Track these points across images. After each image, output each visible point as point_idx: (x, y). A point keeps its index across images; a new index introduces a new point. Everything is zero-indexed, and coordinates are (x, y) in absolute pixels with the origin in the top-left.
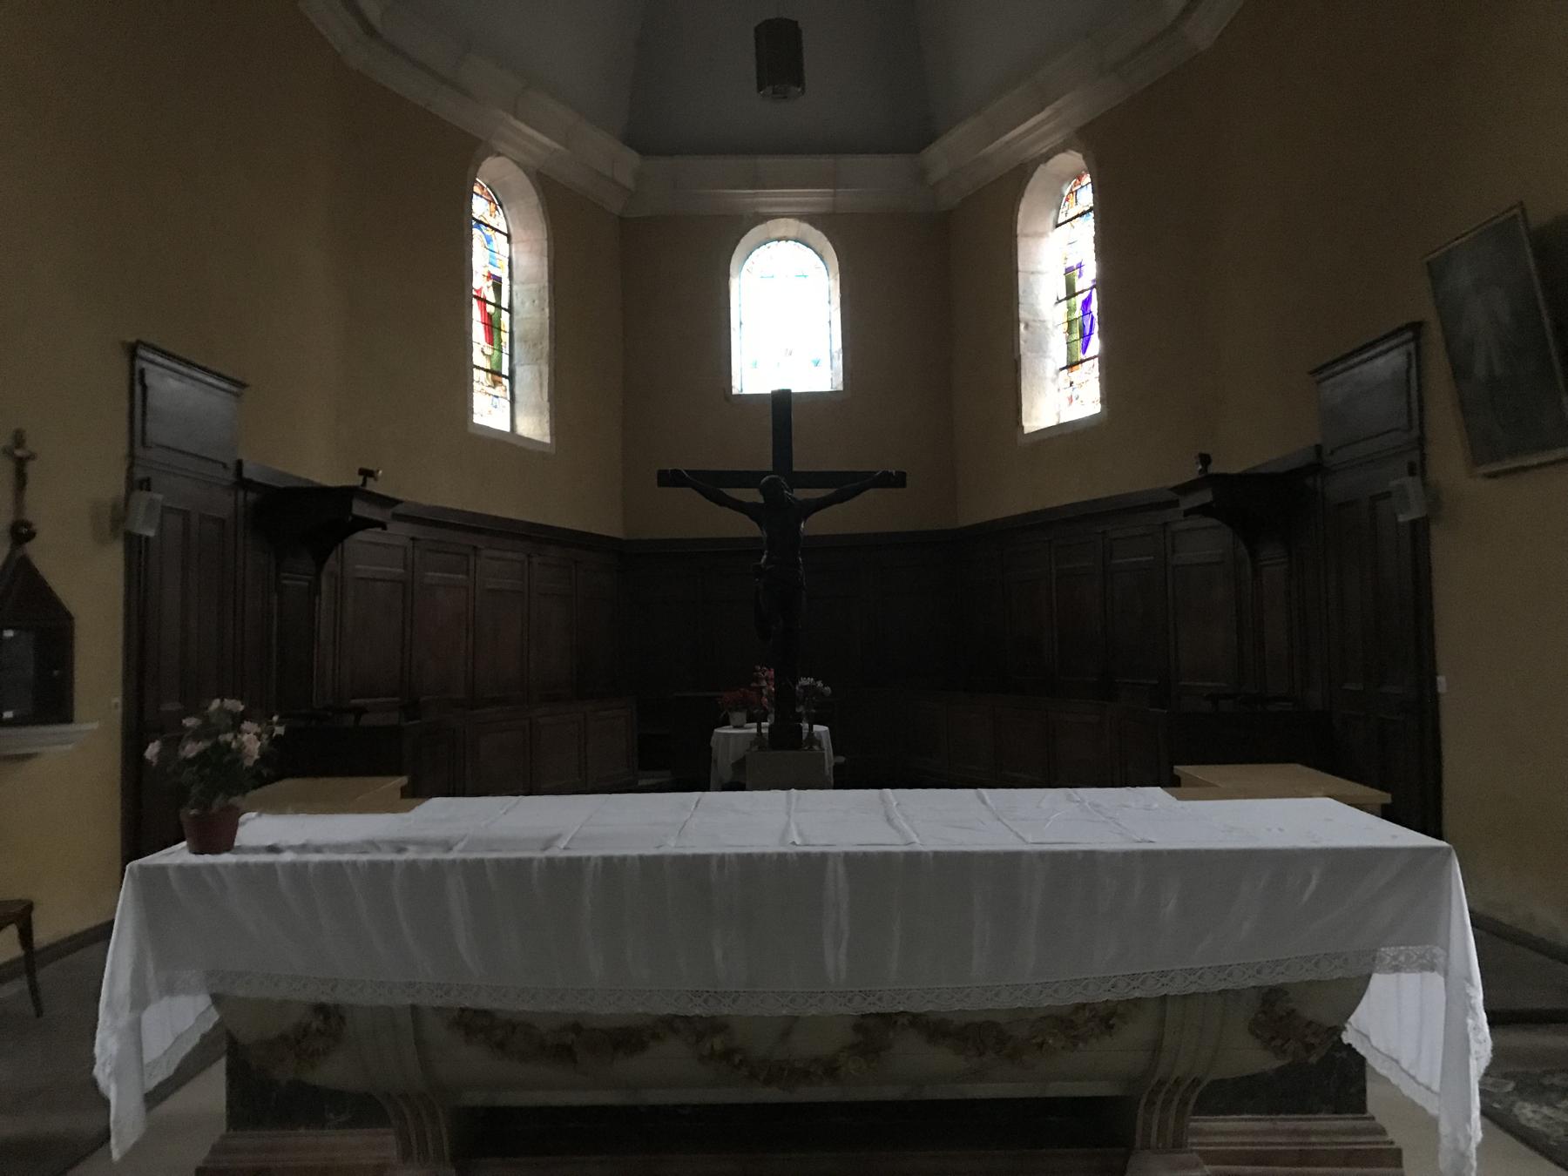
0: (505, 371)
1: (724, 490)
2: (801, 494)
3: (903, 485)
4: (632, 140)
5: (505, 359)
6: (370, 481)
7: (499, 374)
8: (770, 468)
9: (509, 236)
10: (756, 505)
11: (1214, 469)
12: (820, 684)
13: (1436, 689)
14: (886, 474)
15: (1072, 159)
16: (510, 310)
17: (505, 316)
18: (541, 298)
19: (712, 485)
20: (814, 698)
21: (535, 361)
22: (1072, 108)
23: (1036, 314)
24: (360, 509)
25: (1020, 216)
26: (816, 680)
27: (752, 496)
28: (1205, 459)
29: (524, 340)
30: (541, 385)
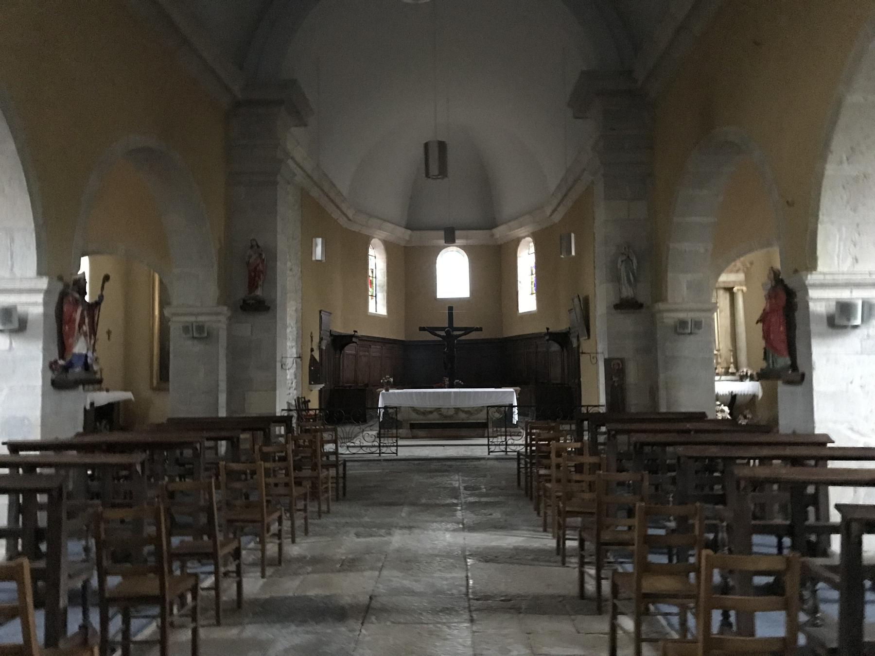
0: (374, 295)
3: (482, 330)
6: (356, 333)
8: (447, 326)
9: (375, 257)
10: (443, 336)
11: (550, 331)
15: (529, 239)
16: (376, 278)
17: (374, 279)
18: (384, 275)
19: (432, 330)
21: (382, 292)
24: (354, 340)
27: (443, 333)
28: (548, 329)
29: (379, 286)
30: (384, 299)
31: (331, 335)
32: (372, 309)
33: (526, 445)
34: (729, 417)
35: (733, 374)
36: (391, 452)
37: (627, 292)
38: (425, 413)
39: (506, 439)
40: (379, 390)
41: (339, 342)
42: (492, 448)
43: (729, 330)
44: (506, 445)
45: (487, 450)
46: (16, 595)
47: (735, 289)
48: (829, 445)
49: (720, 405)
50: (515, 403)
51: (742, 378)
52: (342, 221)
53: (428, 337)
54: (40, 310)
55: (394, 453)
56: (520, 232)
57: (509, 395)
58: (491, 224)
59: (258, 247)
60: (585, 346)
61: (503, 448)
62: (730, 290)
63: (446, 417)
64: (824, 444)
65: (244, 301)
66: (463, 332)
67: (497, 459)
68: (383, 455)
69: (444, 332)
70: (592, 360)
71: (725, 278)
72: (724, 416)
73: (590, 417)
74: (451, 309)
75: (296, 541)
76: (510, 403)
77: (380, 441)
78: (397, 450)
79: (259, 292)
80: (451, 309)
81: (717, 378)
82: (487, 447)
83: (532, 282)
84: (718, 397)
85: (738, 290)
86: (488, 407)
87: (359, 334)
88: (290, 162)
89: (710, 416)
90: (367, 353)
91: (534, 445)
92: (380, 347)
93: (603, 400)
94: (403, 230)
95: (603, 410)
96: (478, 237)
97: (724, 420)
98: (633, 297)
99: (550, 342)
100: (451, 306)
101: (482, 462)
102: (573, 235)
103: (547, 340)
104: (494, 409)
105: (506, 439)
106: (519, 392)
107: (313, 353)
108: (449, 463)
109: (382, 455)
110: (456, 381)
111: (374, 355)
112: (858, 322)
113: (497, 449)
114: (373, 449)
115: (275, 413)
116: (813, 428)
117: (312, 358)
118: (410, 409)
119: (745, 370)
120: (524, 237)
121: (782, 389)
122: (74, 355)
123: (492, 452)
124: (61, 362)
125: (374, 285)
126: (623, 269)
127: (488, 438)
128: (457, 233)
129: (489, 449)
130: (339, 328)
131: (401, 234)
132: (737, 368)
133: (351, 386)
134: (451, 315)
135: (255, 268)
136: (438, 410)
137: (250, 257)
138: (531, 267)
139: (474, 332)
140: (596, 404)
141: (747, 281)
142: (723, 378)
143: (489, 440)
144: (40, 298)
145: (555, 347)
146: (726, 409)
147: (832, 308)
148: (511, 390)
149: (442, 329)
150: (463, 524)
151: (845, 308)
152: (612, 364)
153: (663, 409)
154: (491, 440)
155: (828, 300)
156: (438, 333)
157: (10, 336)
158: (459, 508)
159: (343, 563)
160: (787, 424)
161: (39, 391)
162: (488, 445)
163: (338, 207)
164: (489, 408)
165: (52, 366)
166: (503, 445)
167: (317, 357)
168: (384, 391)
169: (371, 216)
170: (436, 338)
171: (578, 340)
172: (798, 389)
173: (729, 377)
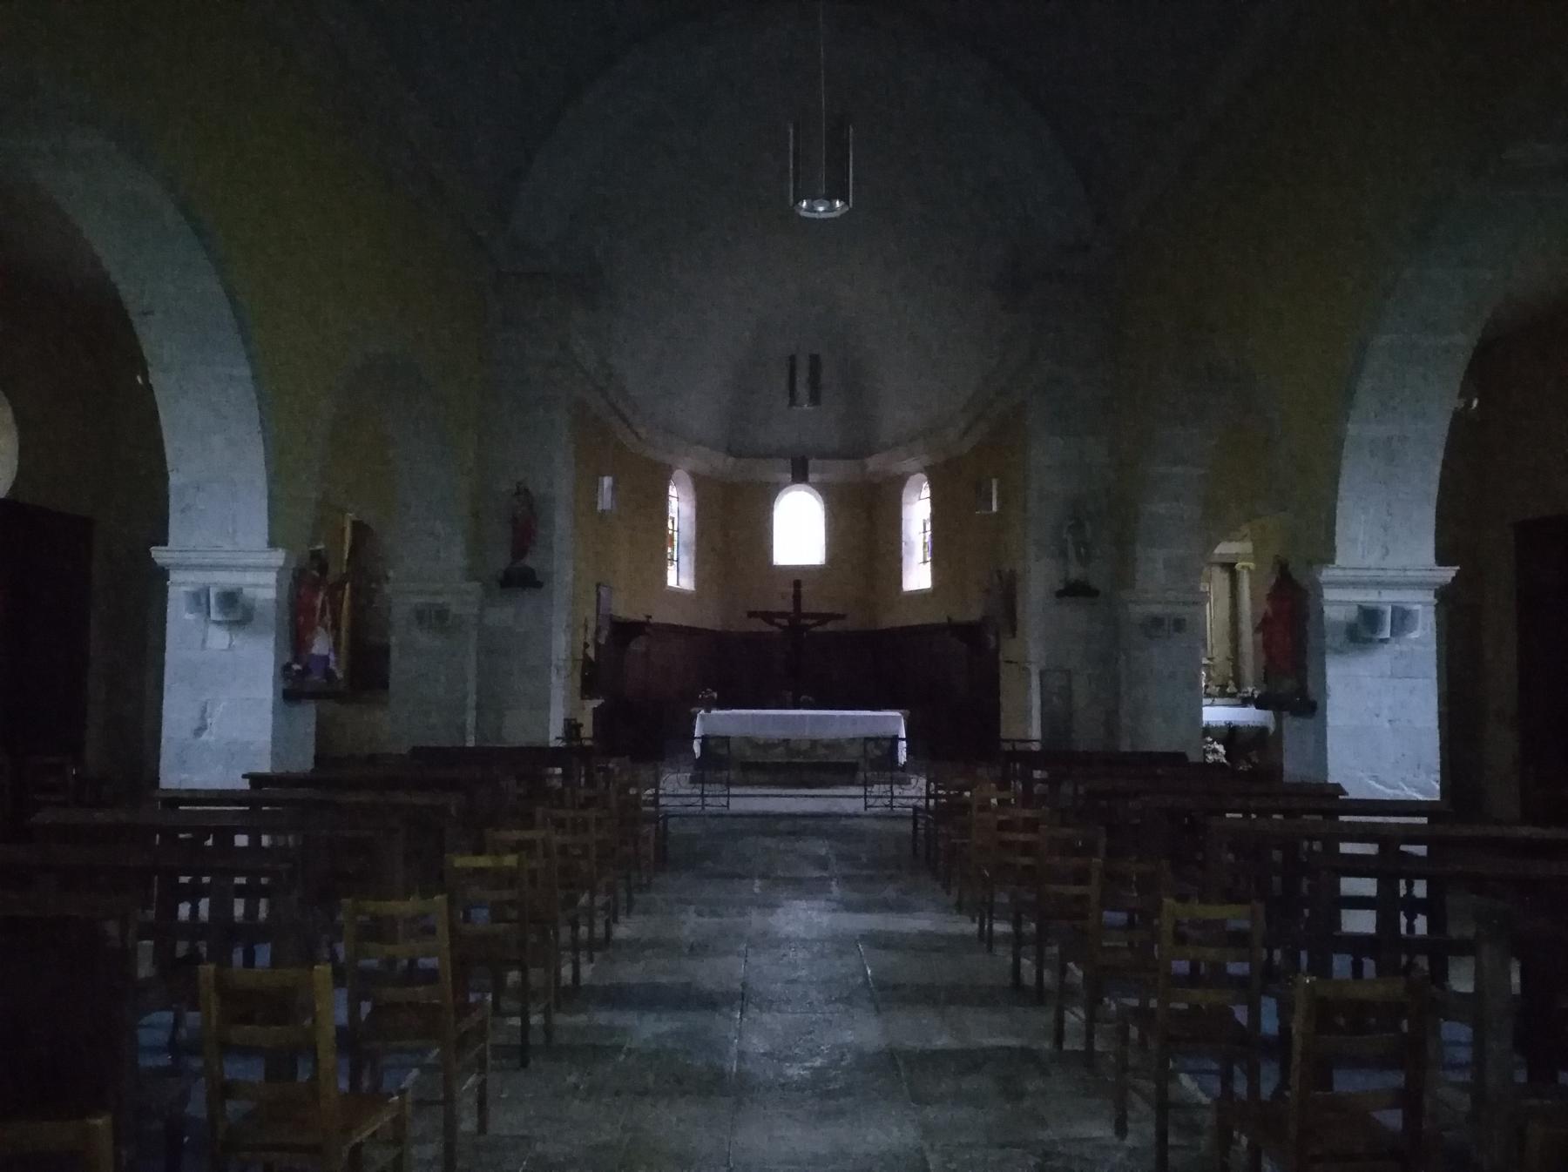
4: (729, 451)
14: (839, 615)
15: (923, 476)
17: (676, 534)
19: (768, 617)
20: (1317, 846)
22: (926, 460)
23: (910, 538)
25: (904, 495)
27: (785, 622)
32: (672, 581)
33: (929, 796)
34: (1225, 761)
35: (1232, 695)
37: (1075, 572)
38: (768, 746)
40: (693, 710)
41: (624, 631)
42: (871, 801)
43: (1227, 627)
44: (892, 797)
45: (864, 803)
47: (1238, 566)
48: (1341, 797)
49: (1212, 743)
50: (903, 734)
51: (1245, 702)
54: (271, 594)
55: (723, 806)
56: (910, 464)
57: (894, 722)
58: (858, 450)
60: (1009, 649)
61: (887, 801)
62: (1229, 567)
63: (799, 753)
66: (814, 621)
67: (877, 817)
71: (1225, 549)
72: (1216, 758)
73: (1014, 756)
74: (797, 584)
75: (619, 920)
79: (529, 562)
80: (797, 584)
81: (1206, 701)
82: (863, 799)
83: (925, 543)
84: (1208, 731)
85: (1243, 567)
87: (654, 620)
89: (1194, 757)
91: (942, 796)
93: (1035, 732)
95: (1036, 747)
96: (839, 471)
97: (1216, 763)
100: (798, 577)
101: (856, 821)
108: (804, 822)
109: (706, 808)
112: (1386, 634)
113: (879, 802)
114: (693, 800)
115: (548, 742)
116: (1326, 774)
117: (585, 655)
118: (871, 745)
119: (1250, 689)
120: (913, 474)
121: (1291, 723)
123: (871, 806)
124: (296, 667)
125: (675, 543)
128: (812, 463)
129: (866, 803)
130: (625, 609)
131: (722, 463)
132: (1238, 685)
134: (797, 597)
136: (787, 741)
138: (924, 520)
140: (1023, 737)
141: (1256, 556)
142: (1217, 701)
143: (866, 789)
144: (271, 578)
146: (1220, 748)
147: (1352, 614)
149: (782, 615)
151: (1370, 617)
153: (1125, 747)
155: (1349, 603)
156: (777, 620)
157: (229, 630)
159: (692, 948)
160: (1293, 768)
161: (269, 705)
165: (284, 671)
166: (887, 797)
168: (702, 712)
170: (775, 628)
172: (1310, 722)
173: (1226, 700)
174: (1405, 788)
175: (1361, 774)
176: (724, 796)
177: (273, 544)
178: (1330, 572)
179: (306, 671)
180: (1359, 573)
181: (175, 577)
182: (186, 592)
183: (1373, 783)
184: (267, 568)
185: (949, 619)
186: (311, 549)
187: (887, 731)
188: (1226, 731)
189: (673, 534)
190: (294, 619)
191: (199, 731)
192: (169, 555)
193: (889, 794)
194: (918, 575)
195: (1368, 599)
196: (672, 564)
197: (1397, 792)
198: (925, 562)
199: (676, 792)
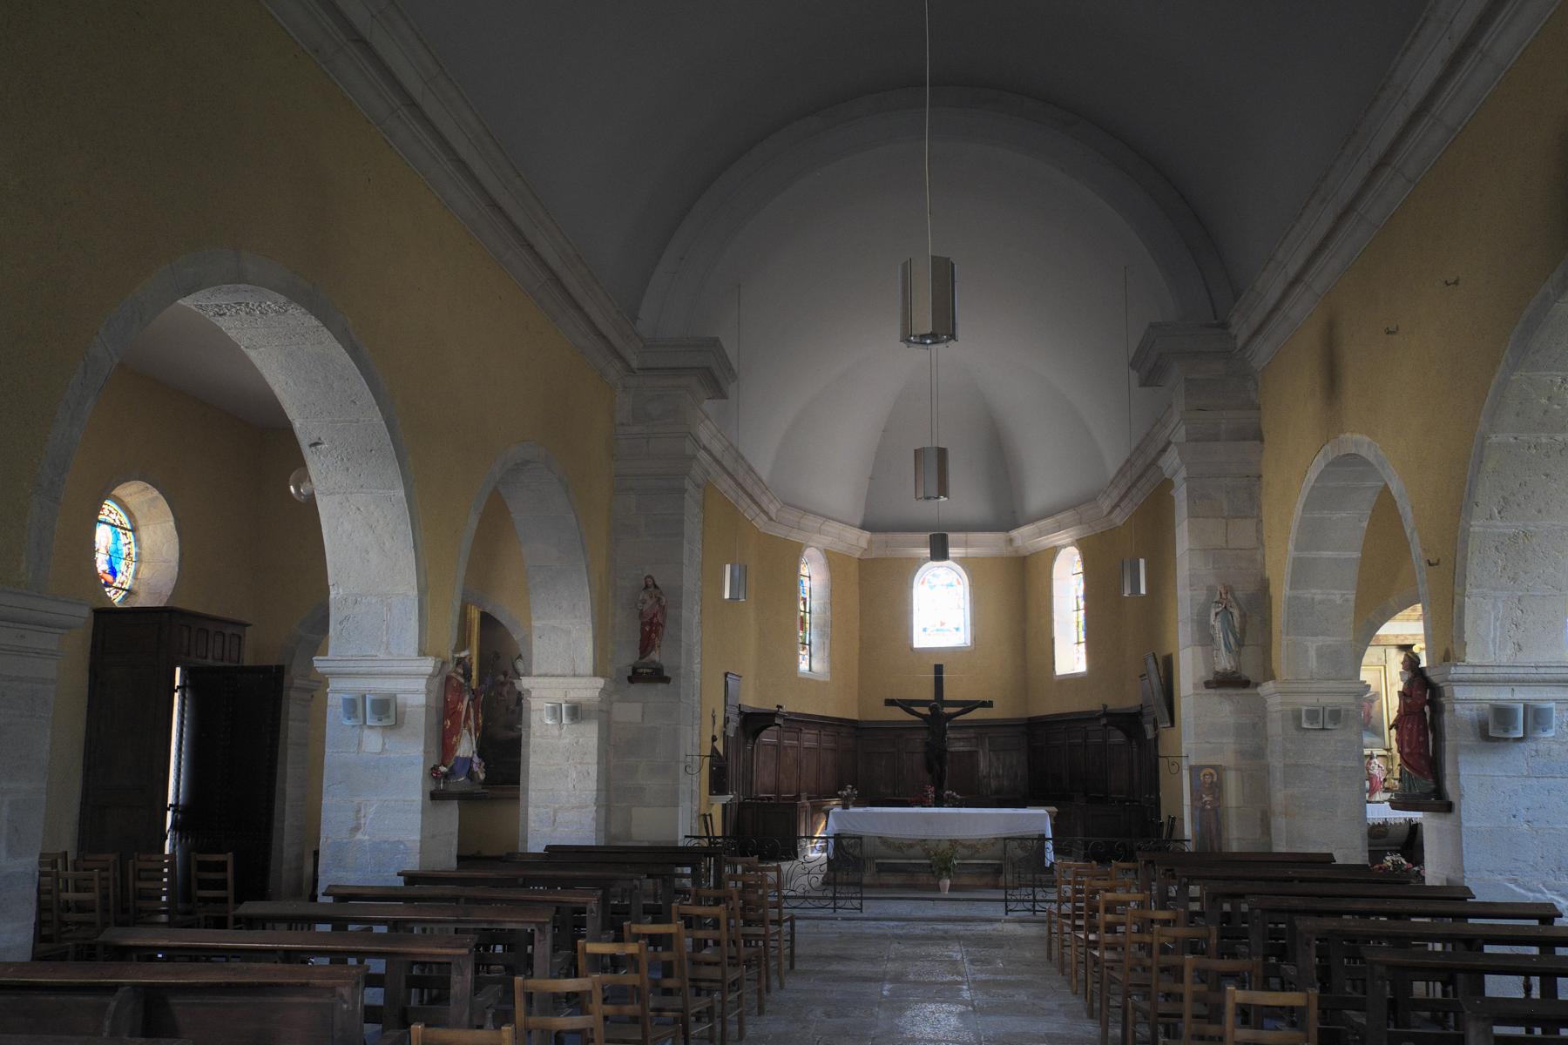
0: (807, 642)
1: (913, 708)
2: (947, 710)
4: (864, 527)
5: (808, 636)
6: (780, 710)
7: (805, 644)
9: (810, 577)
12: (955, 794)
13: (1365, 816)
14: (984, 702)
16: (810, 613)
17: (808, 615)
19: (907, 705)
26: (539, 887)
31: (741, 713)
32: (804, 666)
36: (852, 907)
37: (1224, 662)
39: (1034, 891)
41: (754, 723)
44: (1035, 900)
46: (789, 929)
50: (1049, 834)
52: (760, 522)
53: (898, 714)
59: (656, 587)
64: (1465, 899)
65: (634, 670)
66: (959, 709)
68: (840, 910)
69: (927, 709)
70: (1171, 767)
76: (1041, 833)
77: (835, 889)
78: (861, 905)
80: (939, 669)
86: (1005, 839)
88: (702, 454)
90: (796, 742)
92: (817, 732)
94: (857, 531)
96: (986, 544)
98: (1234, 669)
99: (1109, 728)
100: (939, 665)
102: (1142, 562)
103: (1105, 725)
104: (1015, 844)
105: (1034, 891)
106: (1054, 815)
107: (715, 743)
110: (947, 792)
111: (807, 744)
113: (1020, 906)
115: (677, 841)
117: (714, 749)
120: (1065, 546)
122: (458, 758)
123: (1011, 910)
124: (443, 769)
125: (808, 626)
126: (1218, 625)
127: (1006, 885)
128: (951, 536)
129: (1007, 907)
130: (751, 700)
131: (857, 540)
133: (769, 798)
134: (939, 682)
135: (652, 619)
137: (644, 602)
139: (979, 709)
144: (421, 684)
145: (1118, 737)
148: (1042, 811)
150: (973, 1006)
152: (1202, 775)
154: (1010, 892)
158: (965, 987)
162: (1006, 900)
163: (756, 503)
164: (1008, 841)
166: (1029, 901)
167: (721, 750)
169: (806, 511)
171: (1156, 727)
174: (1545, 890)
175: (1500, 877)
176: (857, 898)
177: (422, 653)
178: (1460, 670)
179: (452, 772)
180: (1490, 670)
181: (334, 684)
182: (344, 699)
183: (1513, 886)
184: (418, 675)
185: (1105, 706)
186: (457, 655)
187: (1031, 829)
188: (1407, 829)
189: (805, 616)
190: (441, 722)
191: (356, 829)
192: (331, 664)
193: (1031, 897)
194: (1071, 657)
195: (1503, 696)
196: (804, 649)
197: (1538, 895)
198: (1078, 643)
199: (807, 894)
